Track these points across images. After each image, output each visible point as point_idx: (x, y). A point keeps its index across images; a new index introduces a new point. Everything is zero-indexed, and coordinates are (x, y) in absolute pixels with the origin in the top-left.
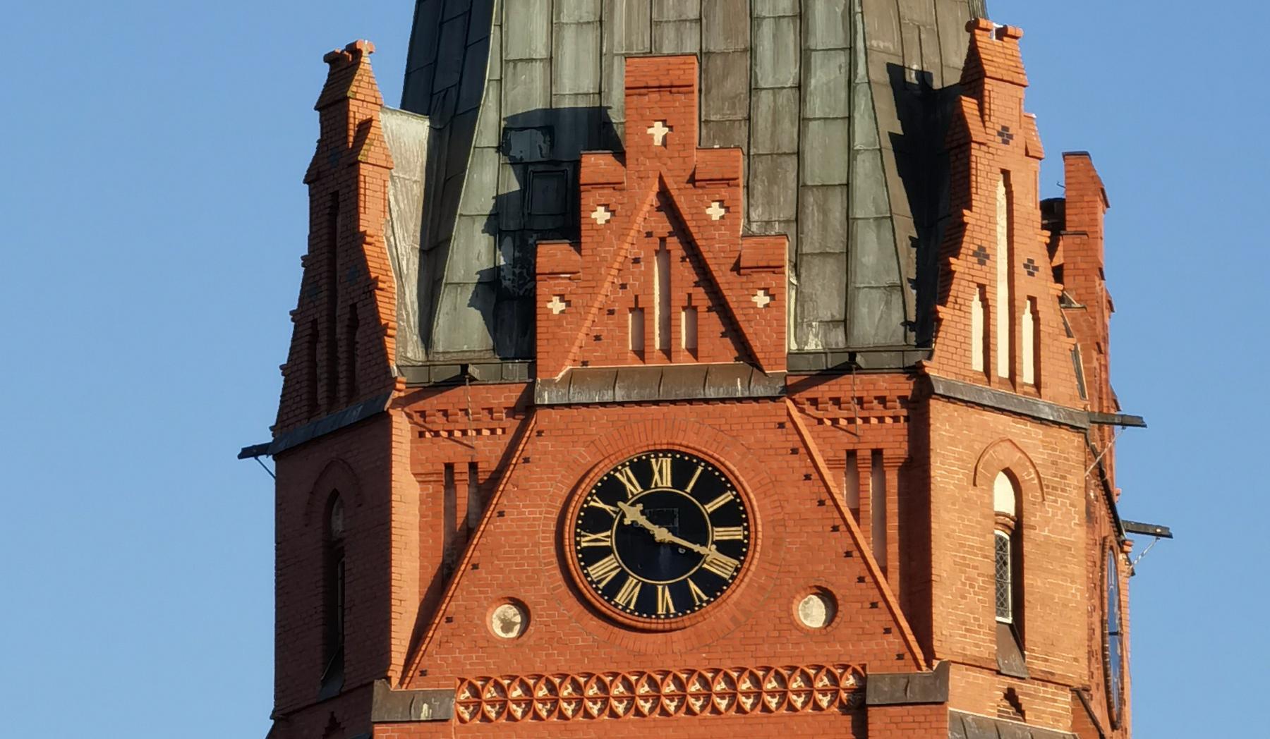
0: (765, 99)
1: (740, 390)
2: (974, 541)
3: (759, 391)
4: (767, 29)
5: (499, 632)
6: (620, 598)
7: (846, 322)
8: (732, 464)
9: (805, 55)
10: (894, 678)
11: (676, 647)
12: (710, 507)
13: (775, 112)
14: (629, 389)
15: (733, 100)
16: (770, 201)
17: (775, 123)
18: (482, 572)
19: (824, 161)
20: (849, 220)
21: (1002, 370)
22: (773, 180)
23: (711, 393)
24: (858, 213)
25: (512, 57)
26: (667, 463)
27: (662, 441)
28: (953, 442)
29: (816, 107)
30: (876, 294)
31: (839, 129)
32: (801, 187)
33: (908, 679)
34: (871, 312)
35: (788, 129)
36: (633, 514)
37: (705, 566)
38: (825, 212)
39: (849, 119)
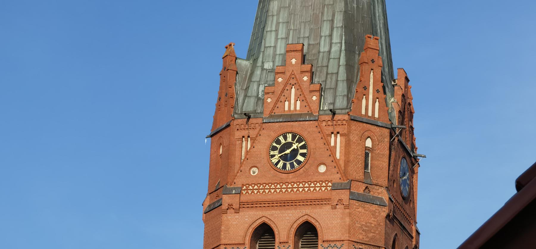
0: (321, 54)
1: (307, 119)
2: (359, 153)
3: (312, 119)
4: (323, 38)
5: (252, 174)
6: (279, 166)
7: (334, 104)
8: (305, 134)
9: (331, 44)
10: (338, 183)
11: (290, 177)
12: (278, 146)
13: (323, 57)
14: (283, 119)
15: (314, 55)
16: (320, 77)
17: (323, 59)
18: (249, 160)
19: (332, 69)
20: (337, 81)
21: (370, 114)
22: (321, 72)
23: (301, 119)
24: (339, 79)
25: (267, 46)
26: (290, 135)
27: (289, 130)
28: (355, 130)
29: (332, 56)
30: (341, 97)
31: (336, 61)
32: (327, 74)
33: (342, 184)
34: (339, 101)
35: (325, 61)
36: (295, 146)
37: (370, 154)
38: (331, 79)
39: (340, 58)
